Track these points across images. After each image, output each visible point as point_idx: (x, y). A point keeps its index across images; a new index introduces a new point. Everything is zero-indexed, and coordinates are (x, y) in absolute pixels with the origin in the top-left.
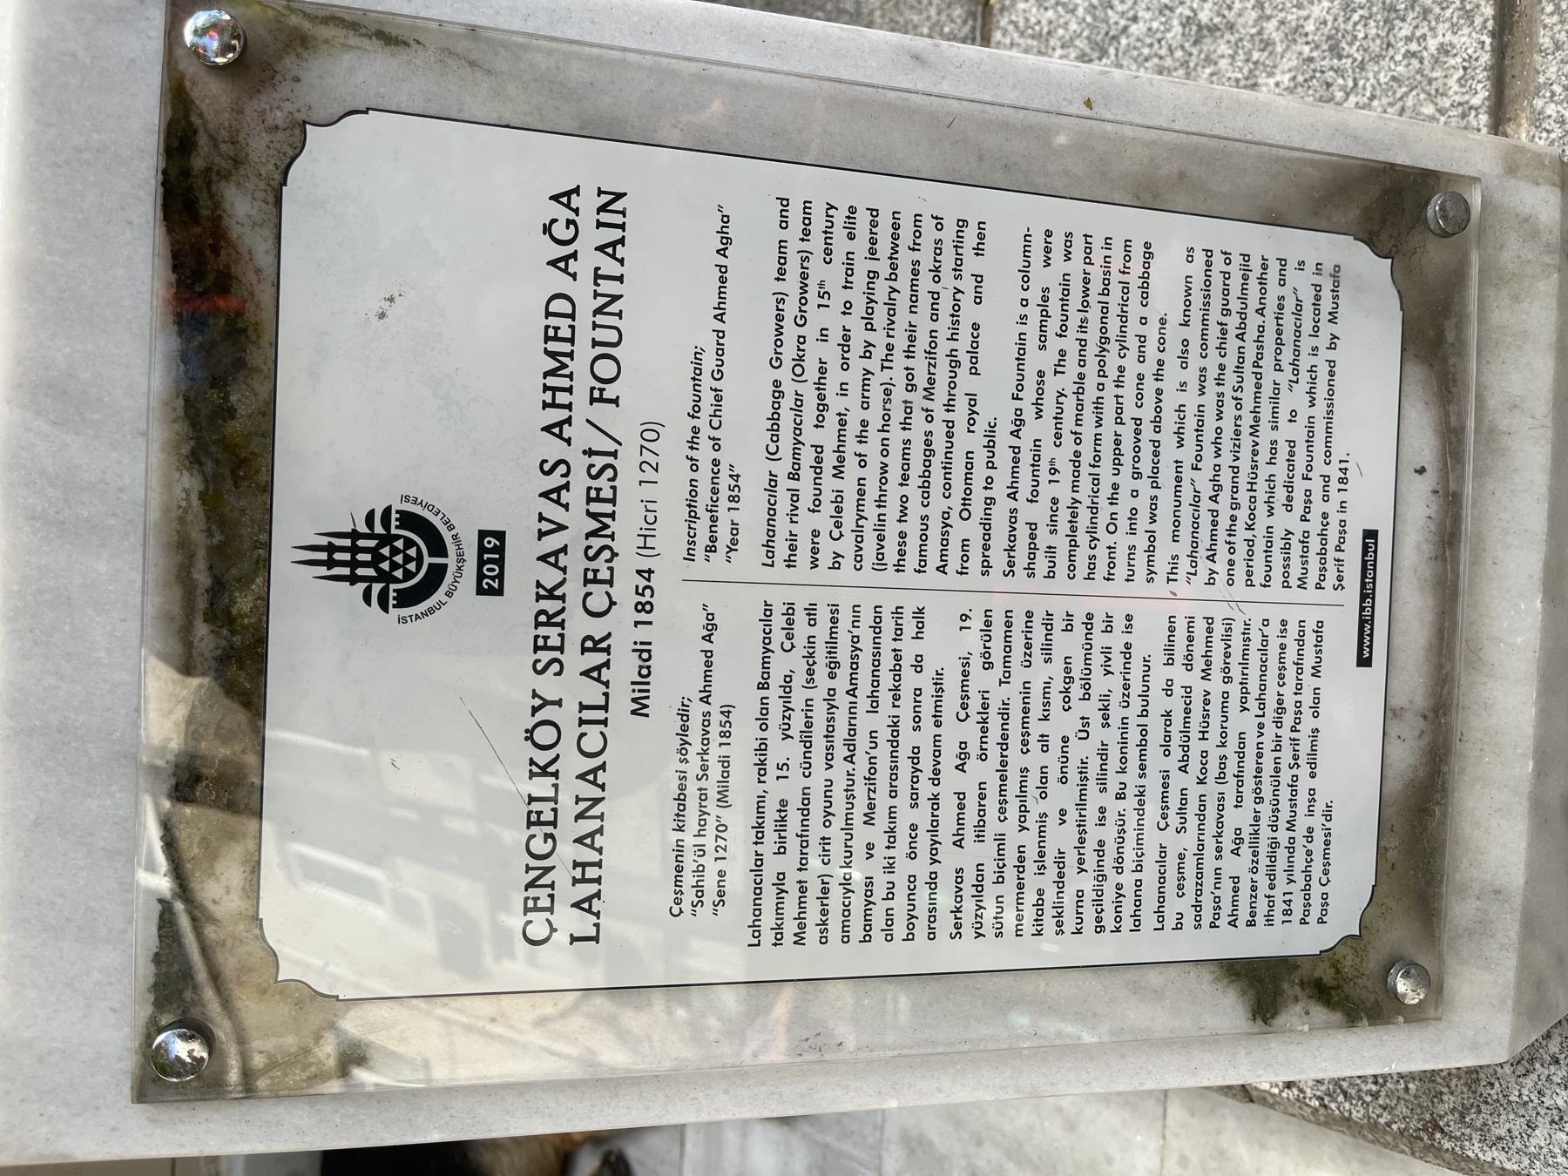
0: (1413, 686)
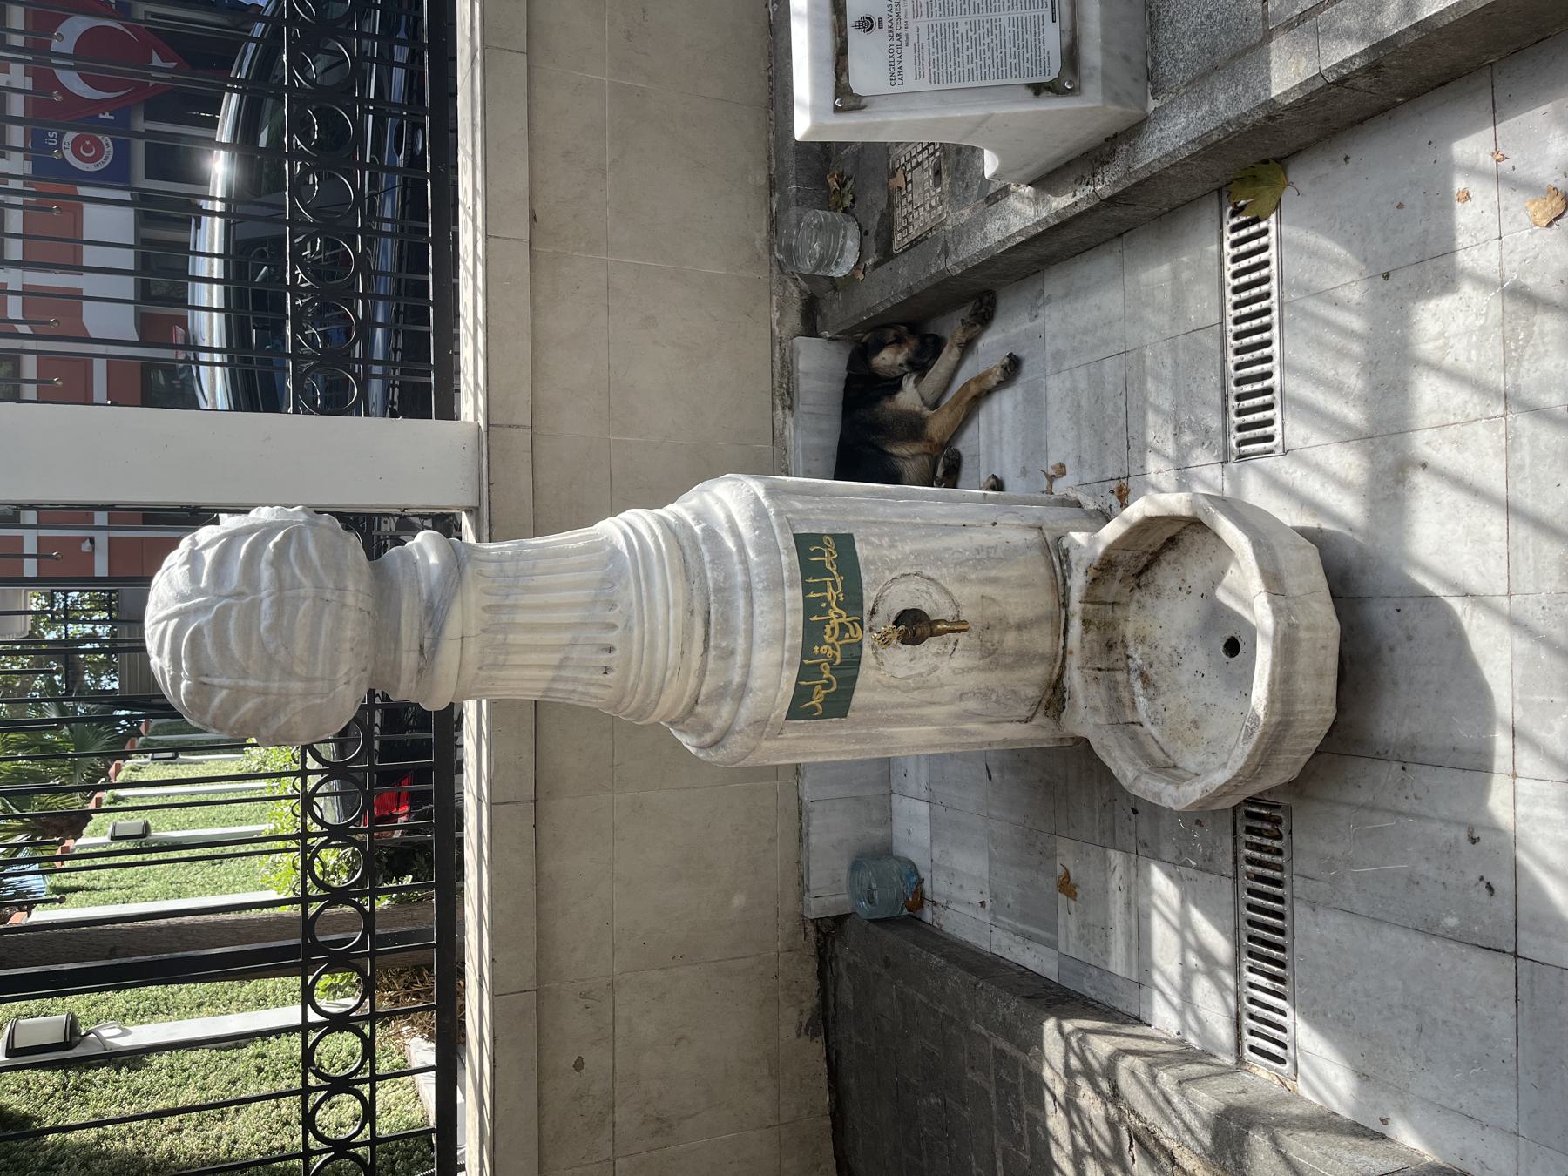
0: (1067, 25)
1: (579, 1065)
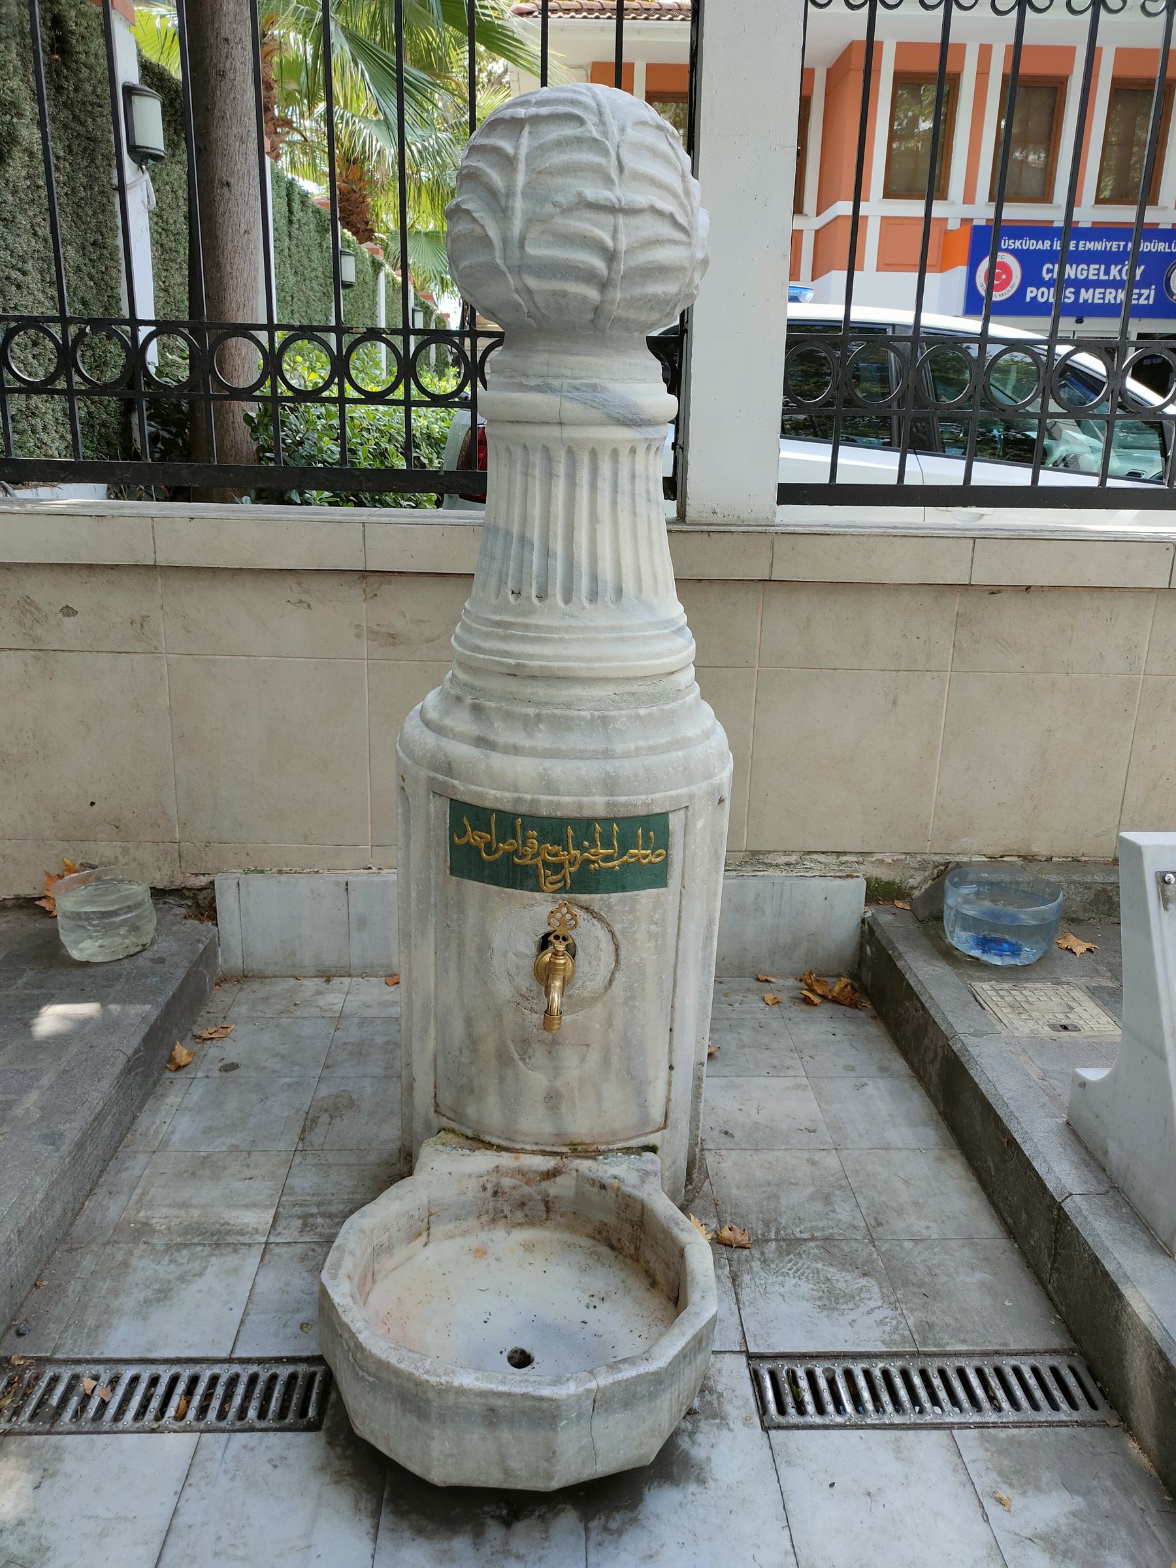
1: (68, 611)
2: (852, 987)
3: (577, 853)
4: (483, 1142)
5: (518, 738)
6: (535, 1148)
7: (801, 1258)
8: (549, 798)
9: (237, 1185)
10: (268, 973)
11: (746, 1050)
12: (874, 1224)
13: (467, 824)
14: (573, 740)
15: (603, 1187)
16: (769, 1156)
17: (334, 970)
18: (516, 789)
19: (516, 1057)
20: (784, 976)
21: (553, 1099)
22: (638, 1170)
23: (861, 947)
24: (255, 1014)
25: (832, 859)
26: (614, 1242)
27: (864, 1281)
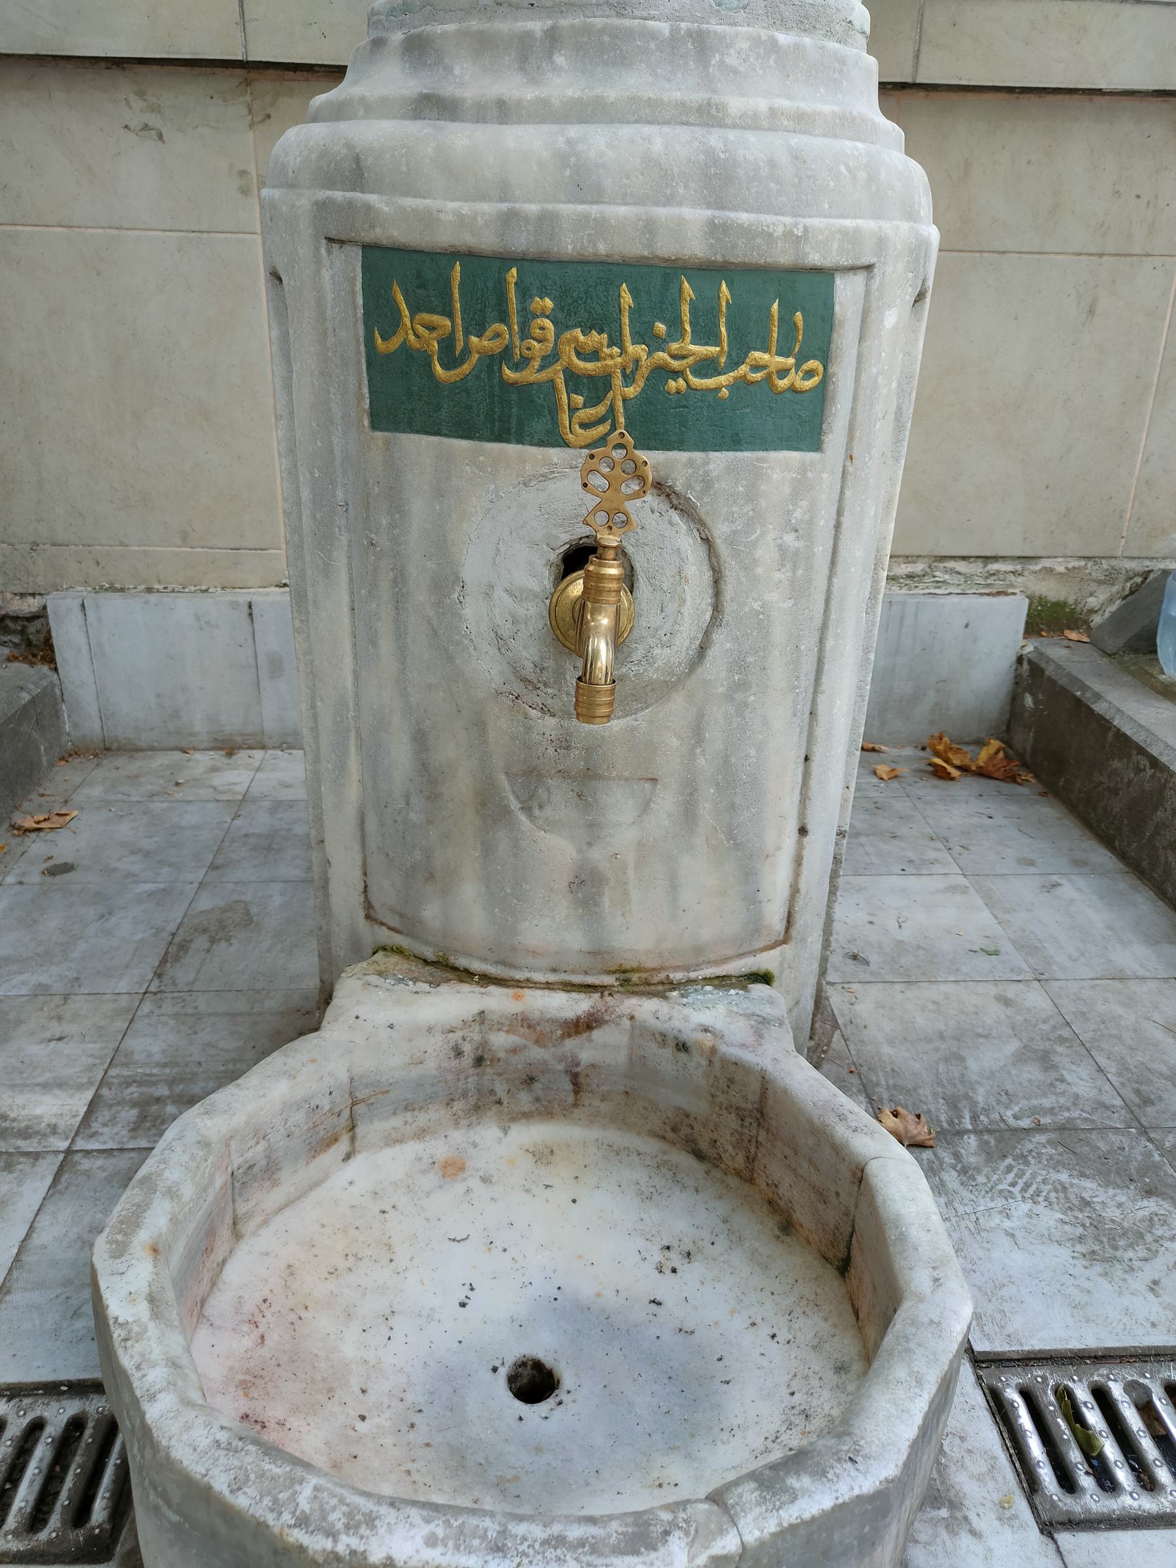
2: (1005, 753)
3: (640, 350)
4: (455, 969)
5: (511, 86)
6: (552, 978)
7: (1027, 1163)
8: (580, 208)
9: (36, 1050)
10: (141, 744)
11: (863, 839)
12: (1137, 1100)
13: (400, 298)
14: (631, 83)
15: (682, 1047)
16: (934, 992)
17: (239, 739)
18: (504, 191)
19: (514, 805)
20: (896, 744)
21: (586, 886)
22: (749, 1016)
23: (1014, 698)
24: (113, 798)
25: (976, 568)
26: (704, 1145)
27: (1151, 1205)
